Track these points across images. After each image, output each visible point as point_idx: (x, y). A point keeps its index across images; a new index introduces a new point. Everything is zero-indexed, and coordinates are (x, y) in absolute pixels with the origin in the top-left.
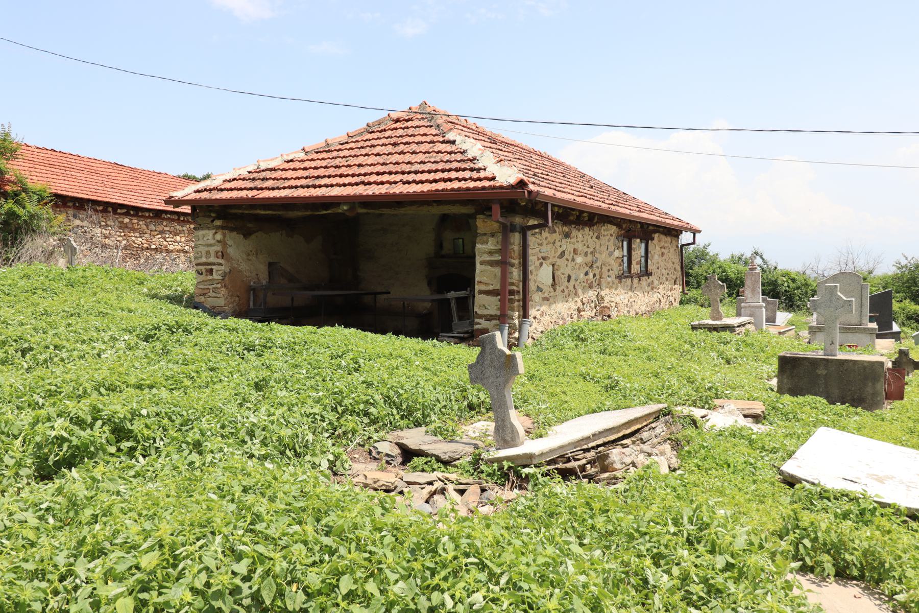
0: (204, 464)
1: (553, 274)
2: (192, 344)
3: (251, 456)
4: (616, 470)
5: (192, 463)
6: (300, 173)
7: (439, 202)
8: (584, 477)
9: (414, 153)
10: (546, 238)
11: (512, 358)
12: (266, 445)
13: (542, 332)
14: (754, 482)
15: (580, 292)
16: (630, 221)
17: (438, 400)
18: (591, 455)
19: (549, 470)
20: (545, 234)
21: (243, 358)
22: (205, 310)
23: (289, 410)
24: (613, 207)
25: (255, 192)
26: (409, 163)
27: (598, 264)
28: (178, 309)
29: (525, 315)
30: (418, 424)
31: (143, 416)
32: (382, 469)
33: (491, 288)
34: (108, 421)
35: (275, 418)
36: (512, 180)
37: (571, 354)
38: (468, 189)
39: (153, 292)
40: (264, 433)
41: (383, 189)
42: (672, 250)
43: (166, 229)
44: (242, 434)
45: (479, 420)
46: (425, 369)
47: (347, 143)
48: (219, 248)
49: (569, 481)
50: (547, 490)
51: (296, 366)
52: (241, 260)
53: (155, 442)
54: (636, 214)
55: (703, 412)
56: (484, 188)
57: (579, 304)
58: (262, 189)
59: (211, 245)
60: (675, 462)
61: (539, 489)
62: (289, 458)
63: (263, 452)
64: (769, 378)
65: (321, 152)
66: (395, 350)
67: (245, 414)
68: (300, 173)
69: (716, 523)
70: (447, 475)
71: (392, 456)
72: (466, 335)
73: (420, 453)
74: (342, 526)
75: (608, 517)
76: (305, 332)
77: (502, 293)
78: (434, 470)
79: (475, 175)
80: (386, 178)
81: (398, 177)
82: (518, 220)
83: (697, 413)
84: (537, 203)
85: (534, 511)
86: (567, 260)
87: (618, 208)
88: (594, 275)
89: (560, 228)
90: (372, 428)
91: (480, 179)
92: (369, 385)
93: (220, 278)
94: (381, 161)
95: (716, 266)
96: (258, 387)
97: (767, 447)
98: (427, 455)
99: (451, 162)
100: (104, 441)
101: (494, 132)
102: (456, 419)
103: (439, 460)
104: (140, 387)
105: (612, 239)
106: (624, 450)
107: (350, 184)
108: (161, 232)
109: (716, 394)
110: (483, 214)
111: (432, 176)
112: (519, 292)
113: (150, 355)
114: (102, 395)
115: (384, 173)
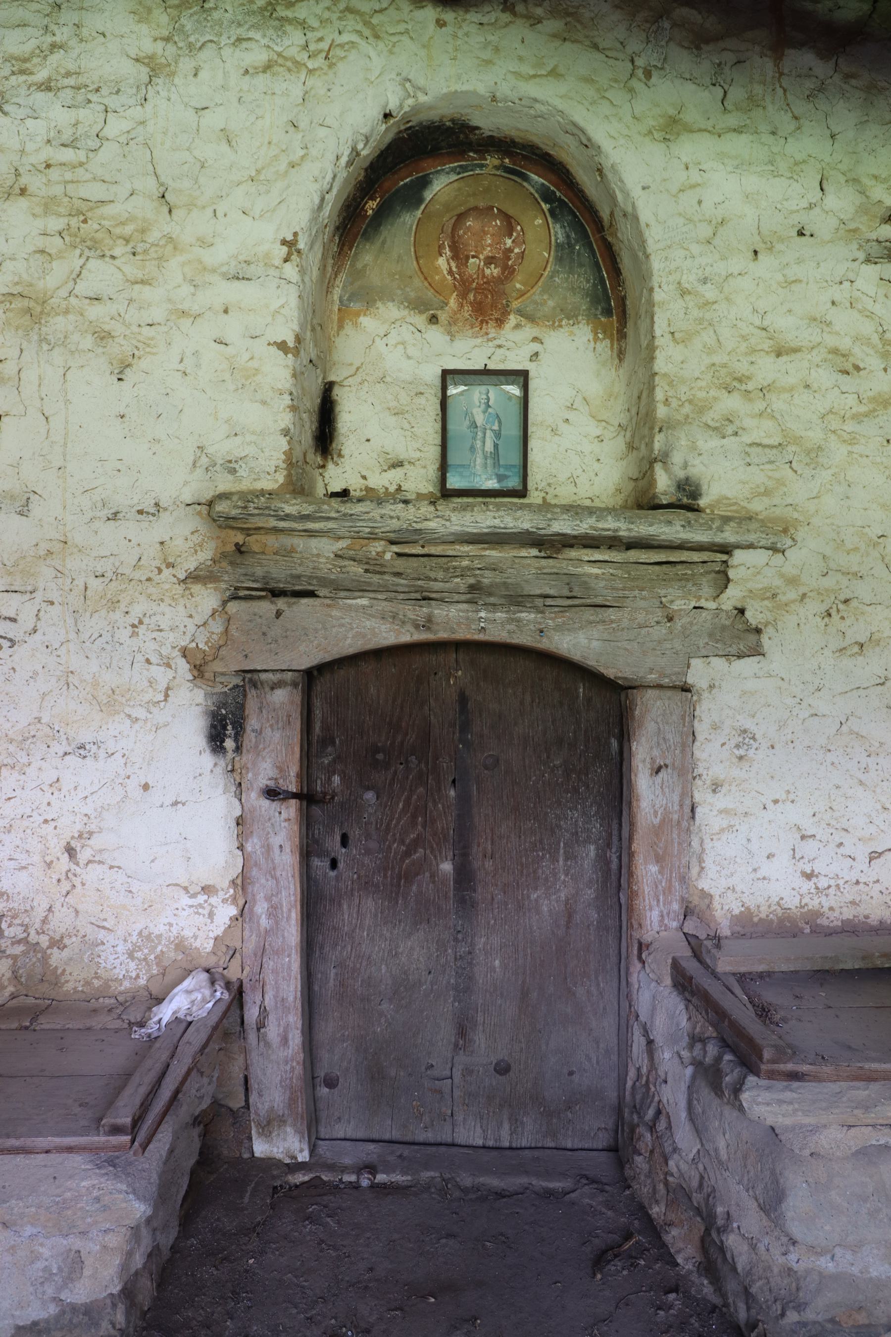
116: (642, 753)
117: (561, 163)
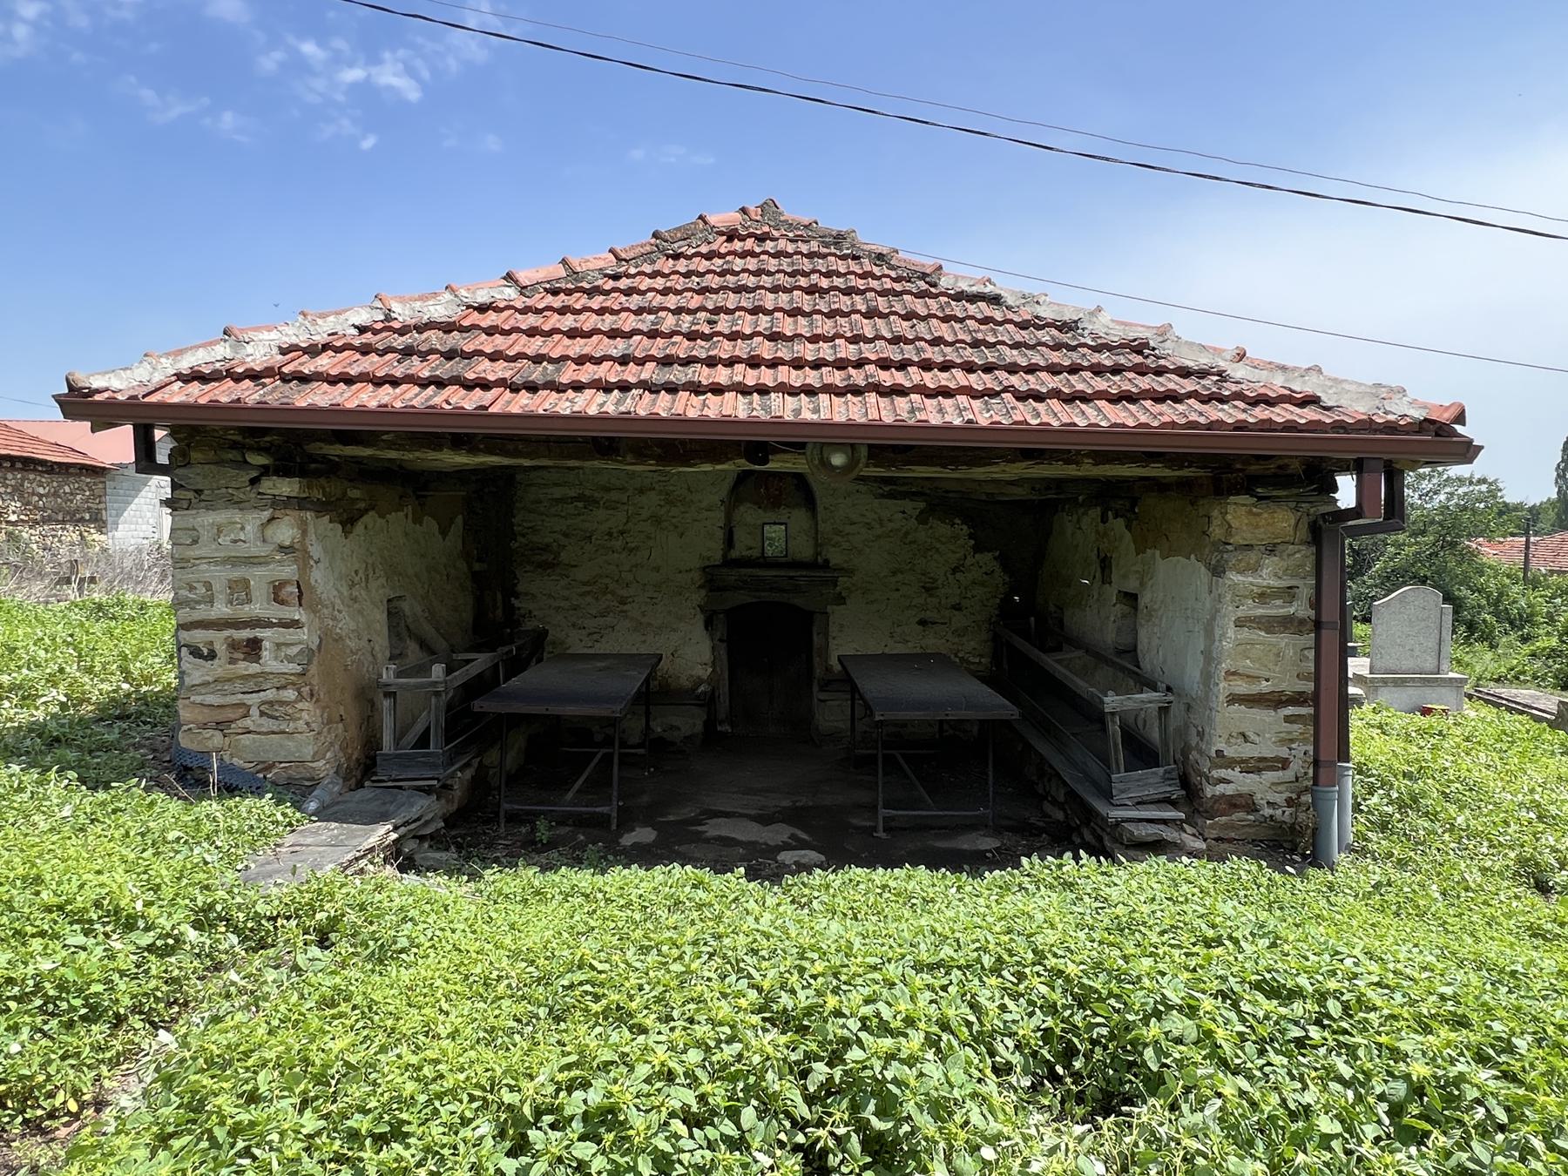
33: (1264, 687)
56: (1290, 426)
59: (251, 561)
81: (1048, 382)
93: (294, 668)
116: (815, 630)
117: (1006, 859)
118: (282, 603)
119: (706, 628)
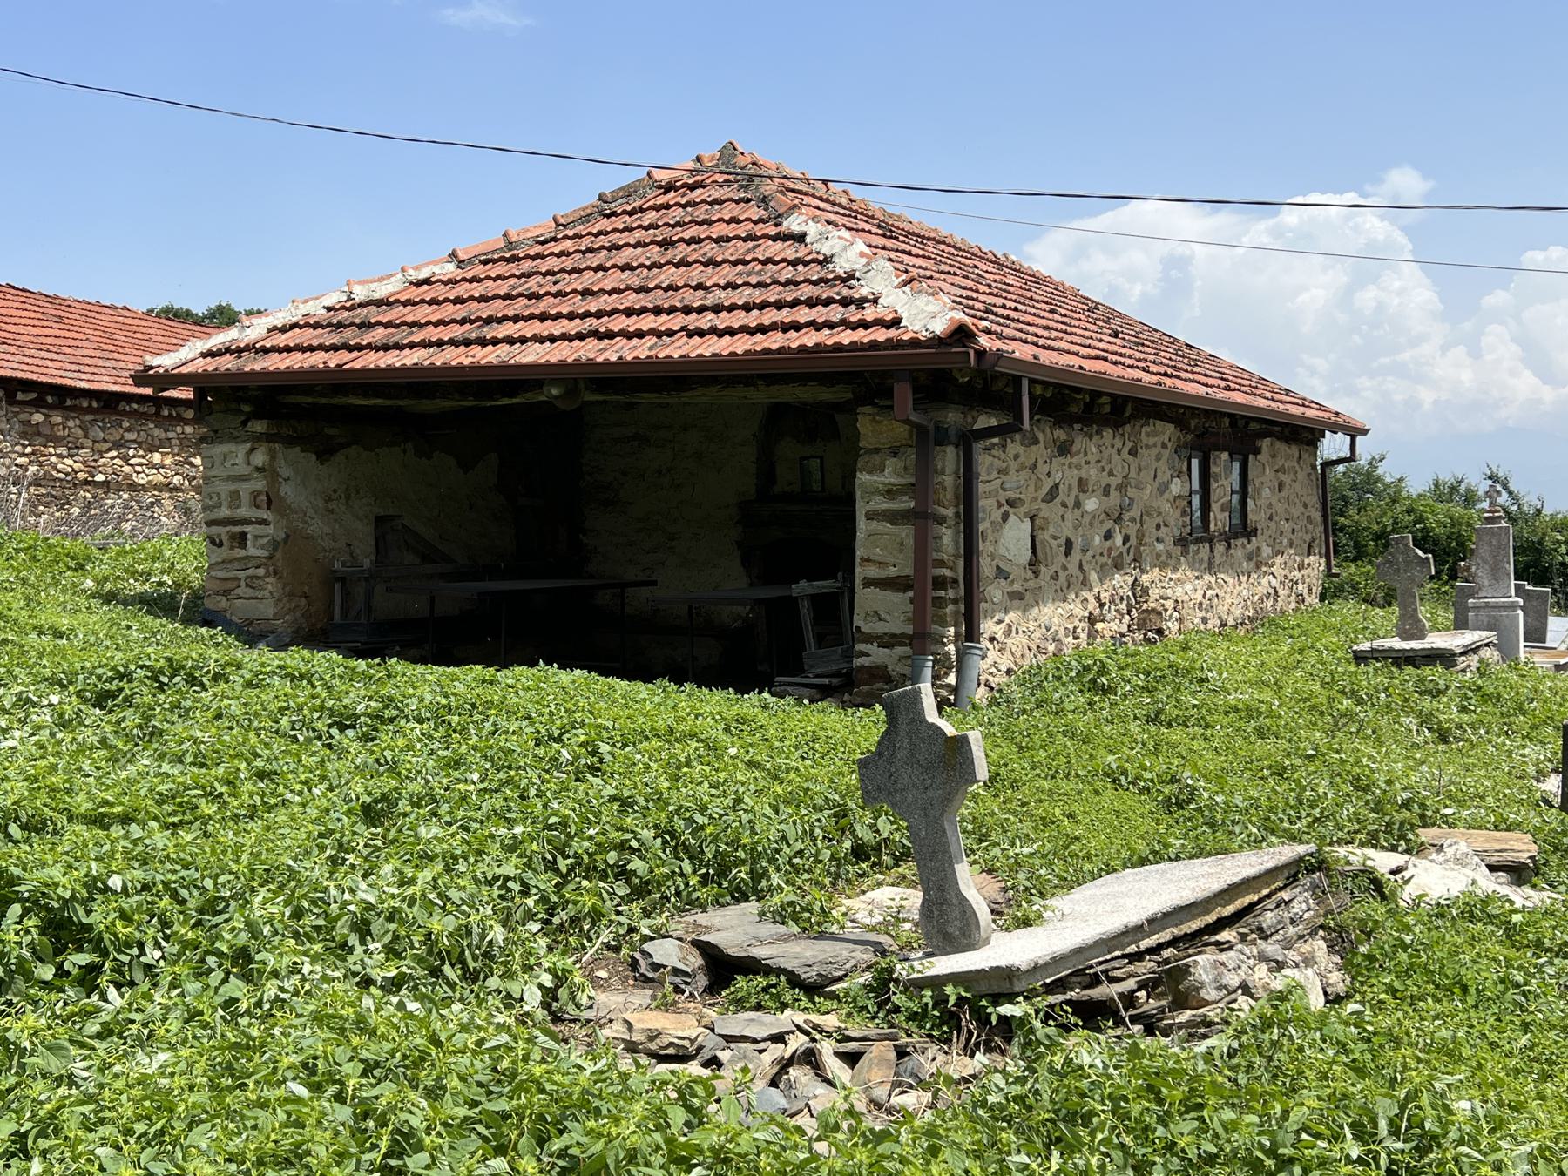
0: (259, 1004)
1: (1033, 537)
2: (209, 715)
3: (366, 982)
4: (1207, 1003)
5: (231, 1002)
6: (448, 311)
7: (772, 379)
8: (1135, 1020)
9: (711, 262)
10: (1016, 457)
11: (961, 743)
12: (398, 955)
13: (1009, 672)
14: (1526, 1027)
15: (1093, 577)
16: (1208, 413)
17: (784, 838)
18: (1146, 967)
19: (1052, 1006)
20: (1014, 447)
21: (329, 746)
22: (229, 628)
23: (448, 869)
24: (1167, 381)
25: (344, 356)
26: (700, 287)
27: (1135, 512)
28: (168, 627)
29: (972, 634)
30: (740, 895)
31: (115, 893)
32: (666, 1007)
33: (892, 572)
34: (33, 904)
35: (417, 889)
36: (939, 327)
37: (1083, 722)
38: (838, 347)
39: (108, 586)
40: (393, 926)
41: (641, 350)
42: (1301, 476)
43: (129, 436)
44: (342, 928)
45: (880, 884)
46: (752, 764)
47: (554, 239)
48: (259, 485)
49: (1099, 1030)
50: (1058, 1059)
51: (456, 763)
52: (310, 512)
53: (142, 952)
54: (1221, 395)
55: (1396, 859)
56: (874, 345)
57: (1093, 605)
58: (359, 348)
60: (1338, 981)
61: (1041, 1056)
62: (452, 985)
63: (393, 973)
64: (1541, 775)
65: (494, 261)
66: (679, 720)
67: (346, 883)
68: (448, 311)
69: (1453, 1135)
70: (816, 1018)
71: (686, 974)
72: (835, 681)
73: (751, 966)
74: (601, 1157)
75: (1202, 1120)
76: (468, 679)
77: (918, 584)
78: (784, 1007)
79: (853, 315)
80: (648, 322)
81: (676, 322)
82: (952, 417)
83: (1383, 861)
84: (996, 376)
85: (1030, 1108)
86: (1064, 505)
87: (1179, 383)
88: (1126, 539)
89: (1048, 434)
90: (636, 908)
91: (865, 325)
92: (625, 804)
94: (636, 283)
95: (1399, 508)
96: (370, 814)
97: (1547, 943)
98: (767, 971)
99: (797, 284)
100: (26, 953)
101: (889, 210)
102: (827, 881)
103: (794, 981)
104: (97, 821)
105: (1166, 453)
106: (1223, 957)
107: (565, 337)
108: (119, 445)
109: (1422, 817)
110: (875, 405)
111: (753, 318)
112: (955, 581)
113: (112, 740)
114: (16, 842)
115: (644, 310)
118: (258, 507)
119: (743, 564)
